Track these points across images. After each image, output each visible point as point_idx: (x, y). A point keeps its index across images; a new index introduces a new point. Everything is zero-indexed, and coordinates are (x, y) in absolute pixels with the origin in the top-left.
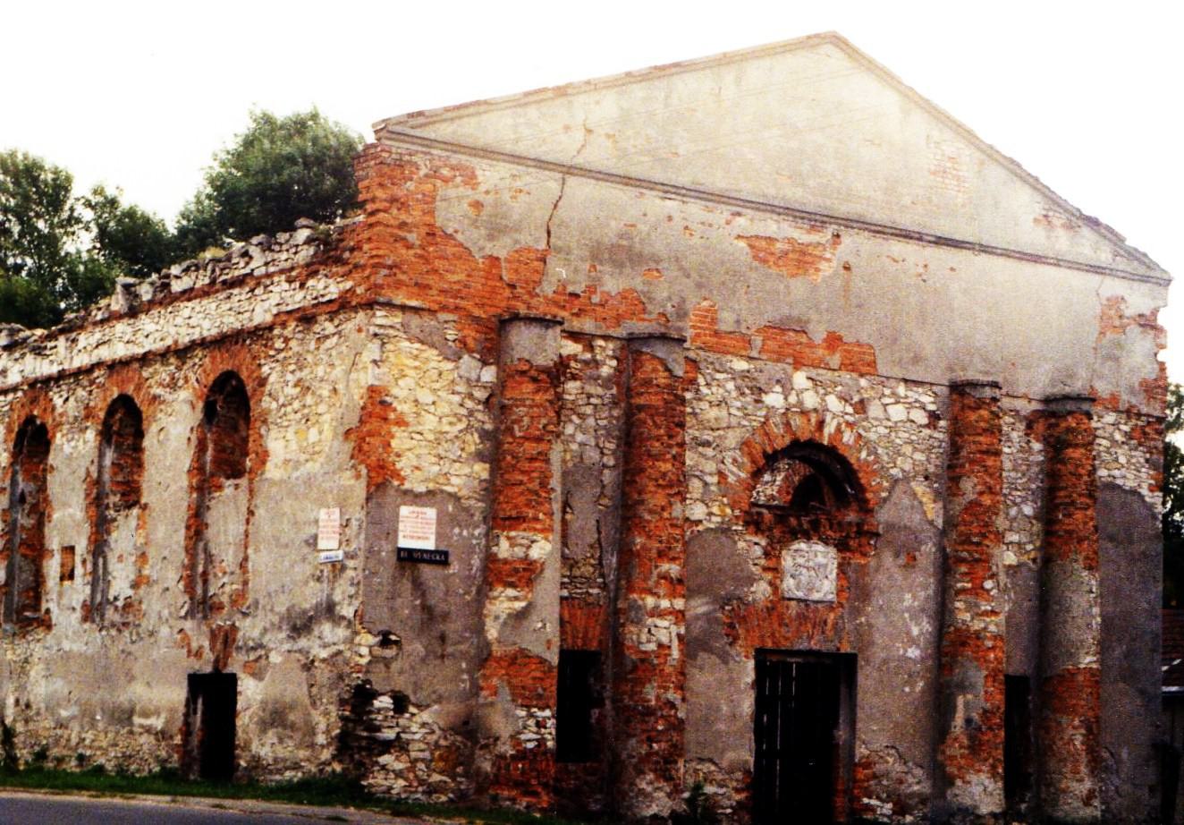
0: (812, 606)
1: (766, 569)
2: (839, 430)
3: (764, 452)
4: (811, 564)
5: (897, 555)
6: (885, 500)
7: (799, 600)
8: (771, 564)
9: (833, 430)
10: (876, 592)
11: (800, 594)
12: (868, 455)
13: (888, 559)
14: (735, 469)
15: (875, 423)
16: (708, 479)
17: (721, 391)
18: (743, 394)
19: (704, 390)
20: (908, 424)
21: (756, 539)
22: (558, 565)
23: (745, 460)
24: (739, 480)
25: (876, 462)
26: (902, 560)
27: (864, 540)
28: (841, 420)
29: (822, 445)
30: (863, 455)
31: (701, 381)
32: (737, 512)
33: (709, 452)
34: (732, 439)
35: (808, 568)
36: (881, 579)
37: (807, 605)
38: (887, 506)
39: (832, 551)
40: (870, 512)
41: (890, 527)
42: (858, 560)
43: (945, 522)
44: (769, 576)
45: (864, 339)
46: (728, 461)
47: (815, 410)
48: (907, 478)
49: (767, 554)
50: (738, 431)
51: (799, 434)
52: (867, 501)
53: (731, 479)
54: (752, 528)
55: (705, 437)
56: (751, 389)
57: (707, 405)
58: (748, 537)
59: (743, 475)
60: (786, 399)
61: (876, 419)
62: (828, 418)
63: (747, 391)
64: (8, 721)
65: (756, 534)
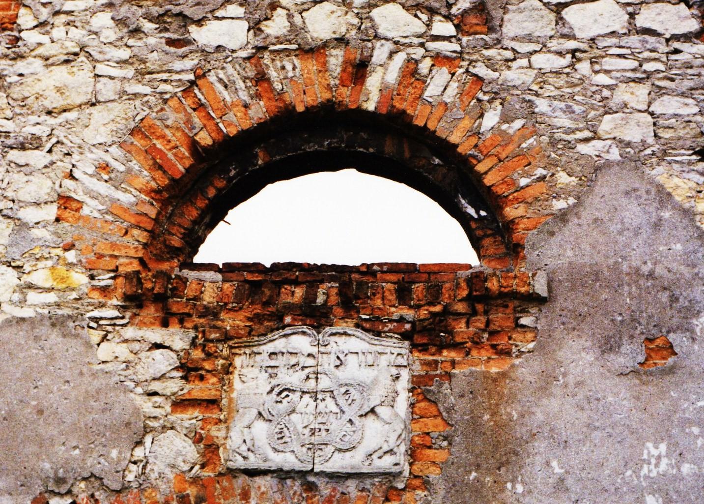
0: (325, 489)
1: (181, 404)
2: (411, 73)
3: (193, 145)
4: (325, 383)
5: (608, 346)
6: (563, 217)
7: (282, 475)
8: (197, 390)
9: (392, 75)
10: (540, 445)
11: (287, 460)
12: (506, 118)
13: (578, 356)
14: (103, 189)
15: (524, 48)
16: (29, 215)
17: (75, 33)
18: (136, 32)
19: (31, 37)
20: (634, 40)
21: (156, 335)
22: (622, 138)
23: (135, 165)
24: (114, 210)
26: (630, 354)
27: (499, 318)
28: (419, 52)
29: (361, 112)
31: (25, 19)
32: (105, 280)
33: (37, 158)
34: (102, 125)
35: (314, 395)
36: (555, 409)
37: (311, 487)
38: (570, 229)
39: (393, 351)
40: (515, 250)
41: (587, 278)
42: (470, 368)
43: (413, 337)
44: (189, 418)
46: (85, 166)
47: (342, 41)
48: (634, 158)
49: (188, 370)
50: (117, 109)
51: (291, 96)
52: (509, 226)
53: (91, 208)
54: (151, 311)
55: (29, 130)
56: (157, 19)
57: (39, 63)
58: (130, 332)
59: (126, 198)
60: (255, 27)
61: (529, 38)
62: (380, 52)
63: (148, 26)
64: (476, 216)
65: (165, 324)
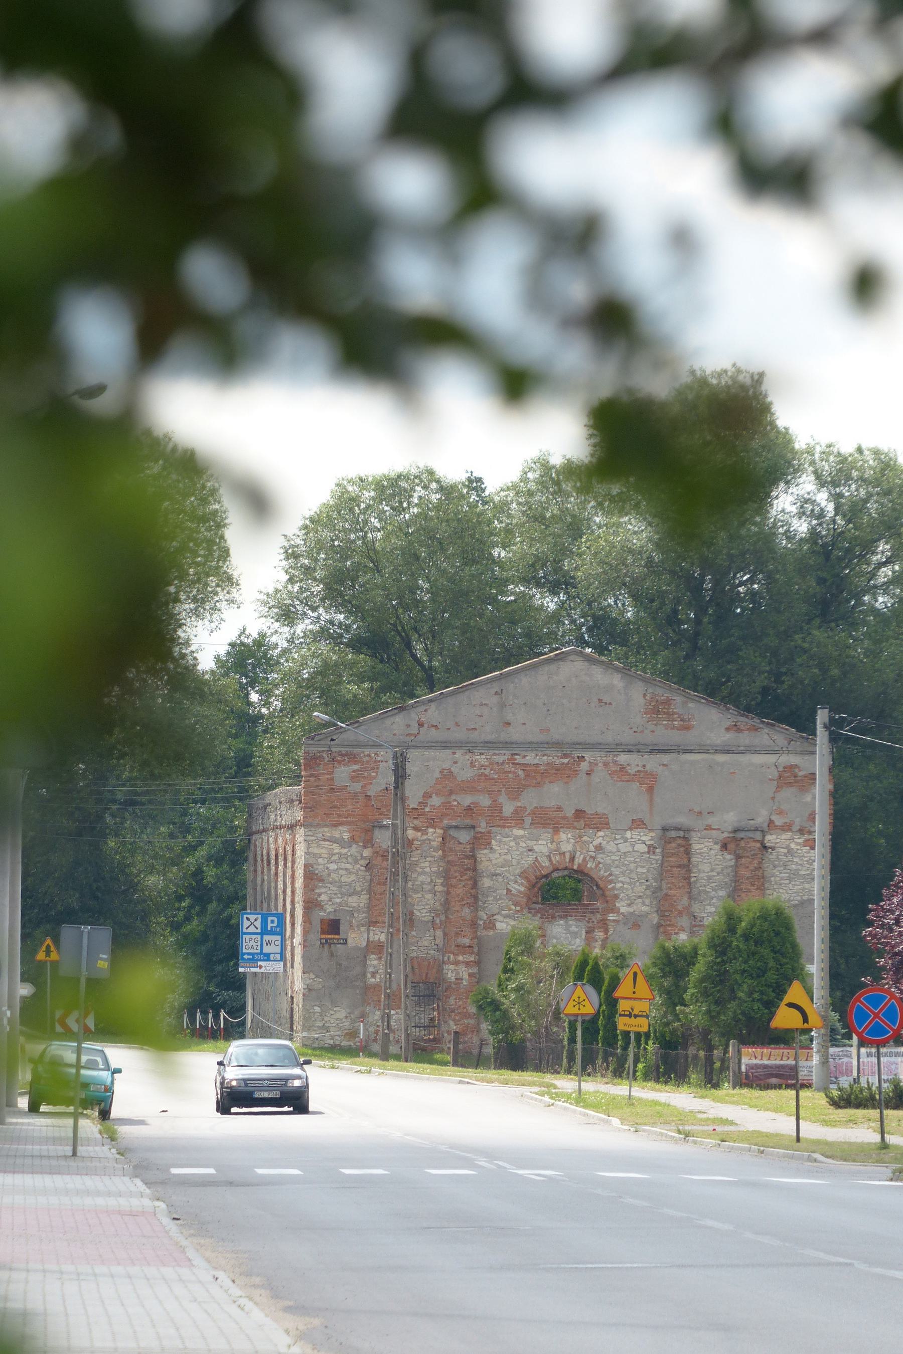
25: (611, 875)
30: (602, 872)
33: (500, 879)
45: (600, 810)
59: (522, 889)
